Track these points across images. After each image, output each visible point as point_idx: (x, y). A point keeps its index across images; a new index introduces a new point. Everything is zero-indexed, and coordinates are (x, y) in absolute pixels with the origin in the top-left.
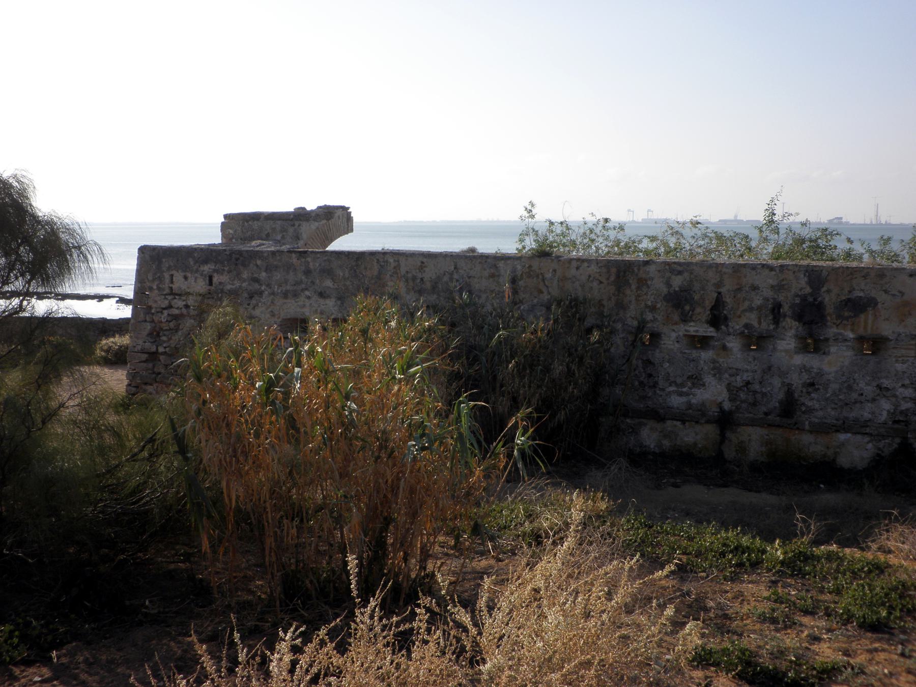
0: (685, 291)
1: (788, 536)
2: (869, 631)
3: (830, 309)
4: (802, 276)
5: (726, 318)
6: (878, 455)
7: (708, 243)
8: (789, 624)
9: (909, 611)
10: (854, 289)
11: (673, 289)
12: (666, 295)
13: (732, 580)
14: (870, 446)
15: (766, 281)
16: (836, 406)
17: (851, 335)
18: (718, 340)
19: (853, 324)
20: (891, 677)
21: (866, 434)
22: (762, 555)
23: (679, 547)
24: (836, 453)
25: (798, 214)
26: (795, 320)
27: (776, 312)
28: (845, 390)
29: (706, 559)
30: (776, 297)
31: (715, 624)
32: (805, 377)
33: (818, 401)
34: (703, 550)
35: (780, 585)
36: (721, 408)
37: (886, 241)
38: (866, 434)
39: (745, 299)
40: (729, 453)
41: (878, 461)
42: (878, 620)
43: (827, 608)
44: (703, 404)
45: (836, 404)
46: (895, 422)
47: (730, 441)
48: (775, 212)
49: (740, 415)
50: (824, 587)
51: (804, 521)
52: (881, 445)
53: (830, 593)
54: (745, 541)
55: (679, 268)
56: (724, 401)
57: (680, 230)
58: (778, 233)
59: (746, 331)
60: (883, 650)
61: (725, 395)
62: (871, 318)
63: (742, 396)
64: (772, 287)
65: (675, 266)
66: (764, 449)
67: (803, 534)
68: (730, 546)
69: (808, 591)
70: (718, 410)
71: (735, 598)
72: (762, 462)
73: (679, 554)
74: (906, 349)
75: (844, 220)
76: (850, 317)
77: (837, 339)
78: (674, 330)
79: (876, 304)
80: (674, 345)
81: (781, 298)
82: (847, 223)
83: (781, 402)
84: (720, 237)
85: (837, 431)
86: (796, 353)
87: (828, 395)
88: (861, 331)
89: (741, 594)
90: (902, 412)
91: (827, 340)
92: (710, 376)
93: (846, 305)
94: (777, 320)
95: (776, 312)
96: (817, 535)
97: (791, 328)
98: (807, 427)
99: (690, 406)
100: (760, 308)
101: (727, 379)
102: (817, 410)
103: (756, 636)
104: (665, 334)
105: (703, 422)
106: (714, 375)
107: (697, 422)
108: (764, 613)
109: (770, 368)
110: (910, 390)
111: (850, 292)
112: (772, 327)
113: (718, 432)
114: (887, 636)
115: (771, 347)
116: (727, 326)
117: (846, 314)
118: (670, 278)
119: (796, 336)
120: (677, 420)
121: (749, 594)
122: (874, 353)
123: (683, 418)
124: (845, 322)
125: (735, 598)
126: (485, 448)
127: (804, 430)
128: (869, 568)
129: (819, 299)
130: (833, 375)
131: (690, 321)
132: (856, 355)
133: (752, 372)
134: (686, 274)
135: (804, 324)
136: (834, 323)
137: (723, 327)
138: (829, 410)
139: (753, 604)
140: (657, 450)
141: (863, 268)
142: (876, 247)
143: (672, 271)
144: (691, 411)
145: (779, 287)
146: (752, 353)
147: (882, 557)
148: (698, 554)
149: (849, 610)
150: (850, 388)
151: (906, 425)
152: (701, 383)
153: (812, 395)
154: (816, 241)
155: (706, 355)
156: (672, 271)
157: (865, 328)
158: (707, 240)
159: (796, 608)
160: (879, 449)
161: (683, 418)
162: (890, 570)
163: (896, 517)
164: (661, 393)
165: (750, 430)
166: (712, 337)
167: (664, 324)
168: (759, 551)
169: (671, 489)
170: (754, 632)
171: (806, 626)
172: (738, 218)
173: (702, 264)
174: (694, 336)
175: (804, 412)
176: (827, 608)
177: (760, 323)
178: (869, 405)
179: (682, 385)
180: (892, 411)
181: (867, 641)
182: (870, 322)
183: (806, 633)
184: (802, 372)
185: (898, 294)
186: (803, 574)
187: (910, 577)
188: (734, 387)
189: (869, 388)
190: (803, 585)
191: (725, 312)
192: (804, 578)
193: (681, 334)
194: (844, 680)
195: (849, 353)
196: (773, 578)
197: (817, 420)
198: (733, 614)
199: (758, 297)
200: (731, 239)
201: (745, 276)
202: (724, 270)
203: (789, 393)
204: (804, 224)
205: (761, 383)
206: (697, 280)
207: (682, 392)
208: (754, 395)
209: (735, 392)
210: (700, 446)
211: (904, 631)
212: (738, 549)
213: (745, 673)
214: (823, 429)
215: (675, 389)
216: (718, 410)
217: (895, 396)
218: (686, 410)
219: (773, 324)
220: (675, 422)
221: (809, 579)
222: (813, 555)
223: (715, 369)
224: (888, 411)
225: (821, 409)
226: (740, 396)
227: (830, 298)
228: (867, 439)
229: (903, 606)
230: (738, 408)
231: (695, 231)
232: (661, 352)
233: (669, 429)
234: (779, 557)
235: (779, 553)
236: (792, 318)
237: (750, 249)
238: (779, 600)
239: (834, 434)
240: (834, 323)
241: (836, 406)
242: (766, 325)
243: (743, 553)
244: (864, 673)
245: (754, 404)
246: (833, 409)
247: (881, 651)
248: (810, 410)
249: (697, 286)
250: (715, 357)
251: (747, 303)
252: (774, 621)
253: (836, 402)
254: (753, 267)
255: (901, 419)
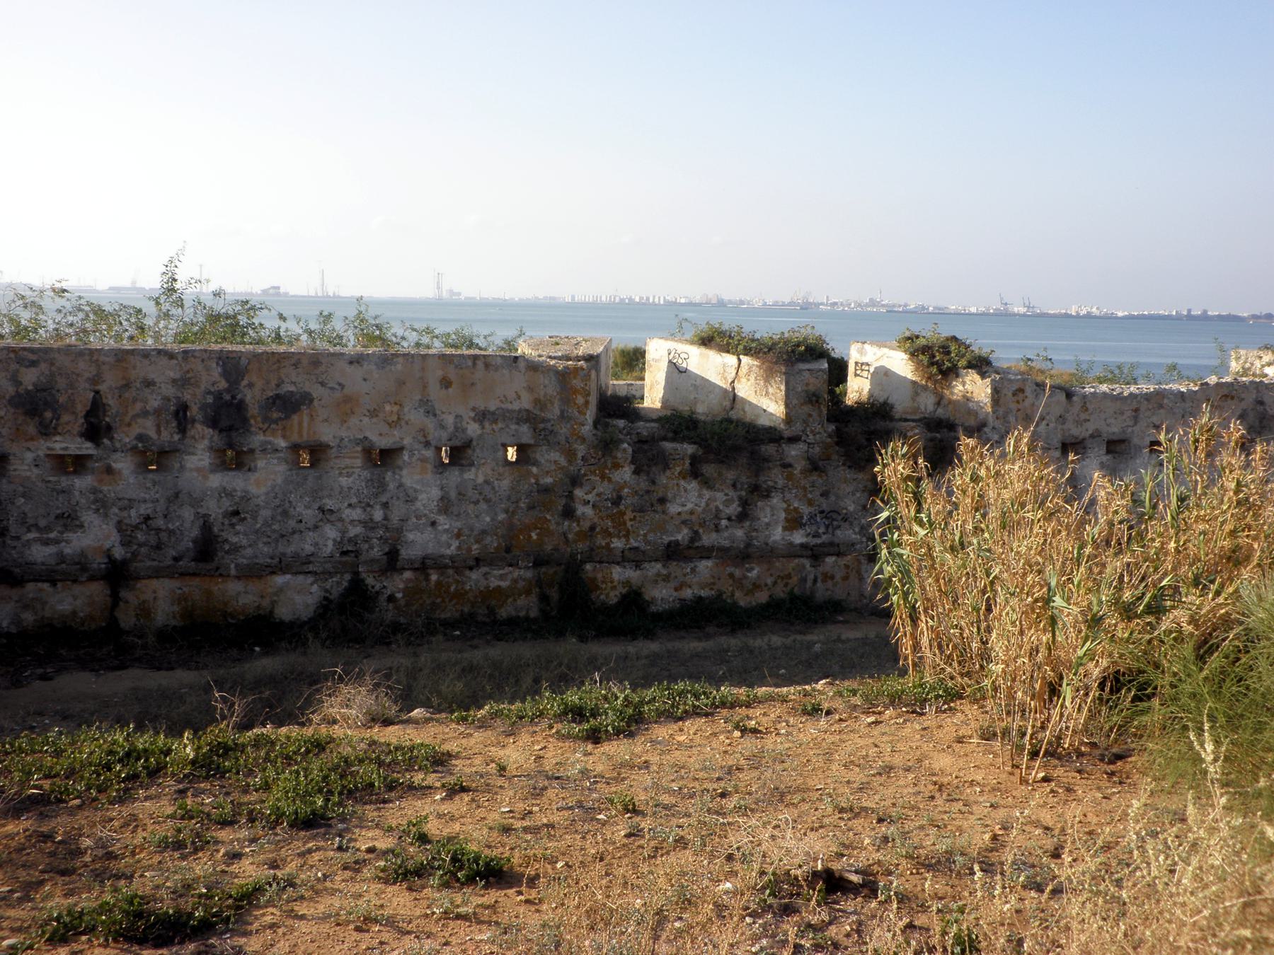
0: (44, 390)
1: (198, 722)
2: (302, 829)
3: (253, 410)
4: (214, 365)
5: (109, 428)
6: (326, 598)
7: (82, 320)
8: (201, 844)
9: (350, 792)
10: (283, 382)
11: (23, 387)
12: (12, 397)
13: (121, 801)
14: (315, 588)
15: (164, 373)
16: (269, 540)
17: (282, 443)
18: (100, 459)
19: (284, 428)
20: (325, 880)
21: (309, 572)
22: (166, 756)
23: (39, 770)
24: (273, 603)
25: (208, 281)
26: (208, 426)
27: (181, 415)
28: (279, 518)
29: (82, 778)
30: (180, 395)
31: (92, 871)
32: (227, 504)
33: (246, 534)
34: (78, 766)
35: (189, 794)
36: (109, 557)
37: (327, 318)
38: (309, 572)
39: (135, 400)
40: (127, 619)
41: (326, 607)
42: (313, 813)
43: (251, 812)
44: (83, 554)
45: (269, 537)
46: (344, 553)
47: (127, 602)
48: (176, 277)
49: (138, 565)
50: (248, 785)
51: (224, 699)
52: (328, 585)
53: (256, 791)
54: (142, 742)
55: (34, 357)
56: (113, 546)
57: (37, 299)
58: (182, 306)
59: (140, 445)
60: (318, 849)
61: (115, 538)
62: (306, 419)
63: (140, 536)
64: (174, 381)
65: (25, 353)
66: (176, 608)
67: (224, 718)
68: (119, 753)
69: (227, 794)
70: (106, 560)
71: (126, 825)
72: (175, 627)
73: (36, 780)
74: (349, 458)
75: (282, 290)
76: (280, 419)
77: (265, 450)
78: (29, 449)
79: (311, 401)
80: (30, 470)
81: (187, 397)
82: (286, 294)
83: (194, 542)
84: (99, 312)
85: (273, 573)
86: (213, 471)
87: (259, 526)
88: (295, 438)
89: (134, 818)
90: (350, 540)
91: (252, 451)
92: (90, 513)
93: (274, 403)
94: (182, 430)
95: (181, 415)
96: (245, 716)
97: (203, 438)
98: (233, 572)
99: (62, 558)
100: (157, 412)
101: (116, 515)
102: (245, 548)
103: (153, 873)
104: (14, 454)
105: (84, 579)
106: (97, 510)
107: (75, 581)
108: (166, 837)
109: (177, 495)
110: (359, 511)
111: (278, 386)
112: (176, 437)
113: (109, 592)
114: (322, 830)
115: (177, 465)
116: (111, 439)
117: (275, 415)
118: (18, 371)
119: (211, 448)
120: (43, 581)
121: (146, 816)
122: (313, 465)
123: (52, 577)
124: (273, 426)
125: (126, 825)
126: (1228, 637)
127: (229, 576)
128: (307, 748)
129: (239, 397)
130: (263, 498)
131: (54, 435)
132: (290, 470)
133: (153, 502)
134: (43, 366)
135: (221, 431)
136: (260, 429)
137: (106, 441)
138: (261, 545)
139: (150, 828)
140: (14, 630)
141: (293, 353)
142: (314, 326)
143: (20, 361)
144: (64, 566)
145: (183, 382)
146: (151, 476)
147: (323, 730)
148: (71, 773)
149: (278, 808)
150: (285, 513)
151: (356, 557)
152: (78, 523)
153: (238, 527)
154: (234, 317)
155: (82, 483)
156: (20, 361)
157: (300, 433)
158: (81, 315)
159: (211, 820)
160: (327, 591)
161: (52, 577)
162: (332, 745)
163: (340, 676)
164: (15, 543)
165: (155, 583)
166: (90, 457)
167: (13, 441)
168: (162, 752)
169: (38, 684)
170: (150, 868)
171: (223, 843)
172: (138, 285)
173: (68, 350)
174: (61, 457)
175: (227, 552)
176: (251, 812)
177: (159, 432)
178: (311, 534)
179: (48, 529)
180: (339, 539)
181: (301, 842)
182: (305, 425)
183: (222, 851)
184: (221, 497)
185: (337, 387)
186: (221, 773)
187: (354, 748)
188: (127, 525)
189: (309, 512)
190: (222, 787)
191: (107, 419)
192: (224, 777)
193: (41, 453)
194: (268, 901)
195: (282, 468)
196: (181, 786)
197: (245, 561)
198: (120, 849)
199: (154, 396)
200: (115, 314)
201: (134, 368)
202: (102, 358)
203: (206, 527)
204: (217, 294)
205: (165, 516)
206: (60, 374)
207: (48, 539)
208: (157, 534)
209: (129, 533)
210: (82, 614)
211: (343, 819)
212: (131, 755)
213: (133, 931)
214: (254, 572)
215: (37, 535)
216: (106, 560)
217: (341, 520)
218: (58, 564)
219: (178, 433)
220: (40, 584)
221: (230, 779)
222: (236, 744)
223: (97, 501)
224: (334, 540)
225: (250, 546)
226: (136, 538)
227: (252, 396)
228: (310, 579)
229: (344, 787)
230: (135, 555)
231: (60, 302)
232: (10, 482)
233: (31, 596)
234: (188, 755)
235: (188, 750)
236: (203, 423)
237: (142, 329)
238: (188, 815)
239: (269, 577)
240: (260, 429)
241: (269, 540)
242: (169, 435)
243: (138, 759)
244: (293, 885)
245: (158, 547)
246: (265, 543)
247: (315, 851)
248: (236, 549)
249: (61, 383)
250: (96, 484)
251: (139, 406)
252: (179, 845)
253: (269, 533)
254: (146, 354)
255: (350, 548)
